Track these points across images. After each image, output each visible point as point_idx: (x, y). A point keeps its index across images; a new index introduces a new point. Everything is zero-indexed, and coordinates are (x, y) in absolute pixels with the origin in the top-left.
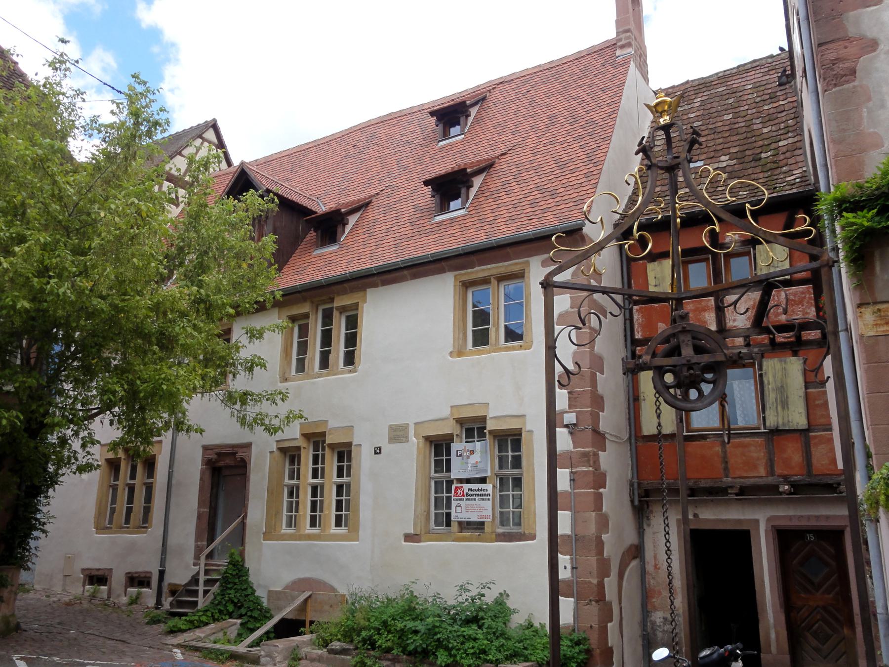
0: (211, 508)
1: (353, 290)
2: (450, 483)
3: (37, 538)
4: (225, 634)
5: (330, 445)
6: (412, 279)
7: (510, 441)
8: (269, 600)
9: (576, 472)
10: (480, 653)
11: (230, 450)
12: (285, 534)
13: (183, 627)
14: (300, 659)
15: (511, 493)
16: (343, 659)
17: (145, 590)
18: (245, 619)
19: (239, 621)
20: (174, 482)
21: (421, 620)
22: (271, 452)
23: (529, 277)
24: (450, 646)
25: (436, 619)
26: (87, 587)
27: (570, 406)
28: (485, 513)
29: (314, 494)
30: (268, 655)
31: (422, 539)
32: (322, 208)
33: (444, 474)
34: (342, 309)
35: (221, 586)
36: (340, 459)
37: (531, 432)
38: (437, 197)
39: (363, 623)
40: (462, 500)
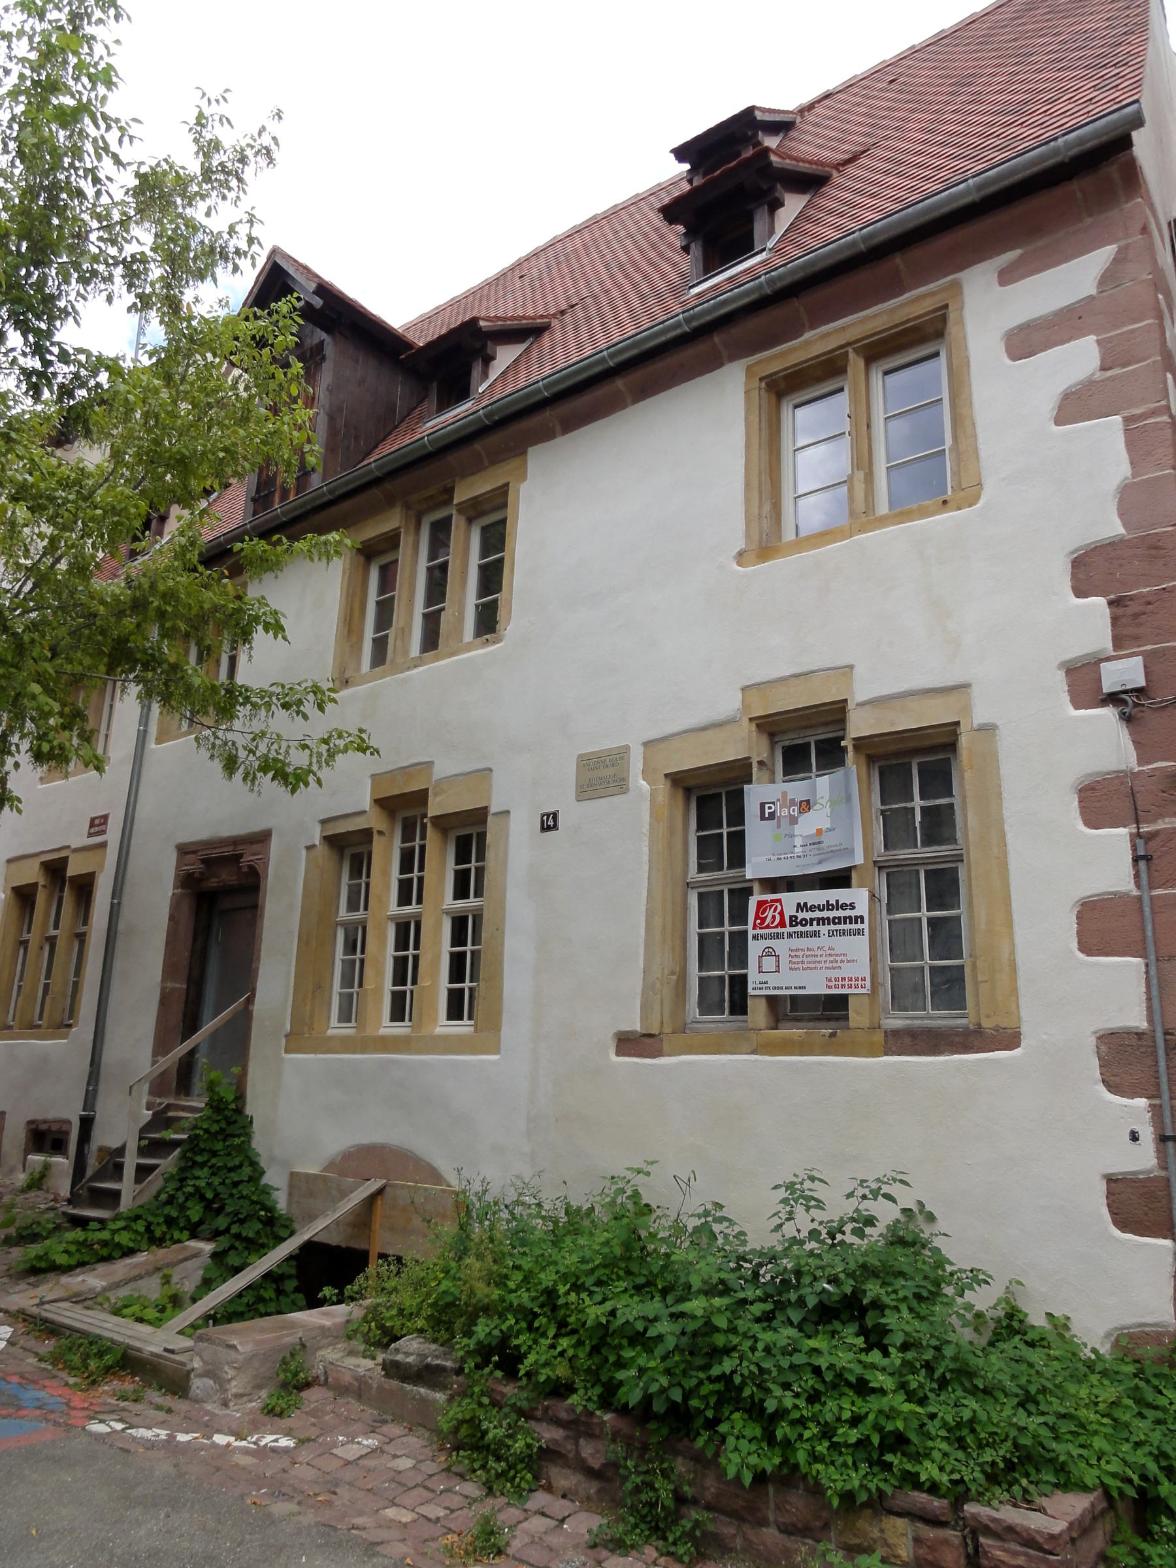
0: (189, 980)
1: (496, 458)
2: (741, 894)
4: (167, 1280)
5: (437, 820)
7: (920, 767)
8: (290, 1195)
9: (1150, 837)
10: (883, 1448)
11: (228, 851)
13: (62, 1259)
14: (307, 1385)
15: (924, 914)
16: (423, 1400)
17: (58, 1159)
18: (224, 1242)
19: (208, 1247)
20: (122, 926)
21: (664, 1292)
22: (309, 848)
24: (771, 1405)
25: (717, 1302)
27: (1119, 641)
28: (847, 971)
30: (211, 1373)
31: (666, 1047)
33: (725, 873)
34: (473, 510)
35: (183, 1156)
36: (462, 856)
37: (989, 729)
39: (486, 1293)
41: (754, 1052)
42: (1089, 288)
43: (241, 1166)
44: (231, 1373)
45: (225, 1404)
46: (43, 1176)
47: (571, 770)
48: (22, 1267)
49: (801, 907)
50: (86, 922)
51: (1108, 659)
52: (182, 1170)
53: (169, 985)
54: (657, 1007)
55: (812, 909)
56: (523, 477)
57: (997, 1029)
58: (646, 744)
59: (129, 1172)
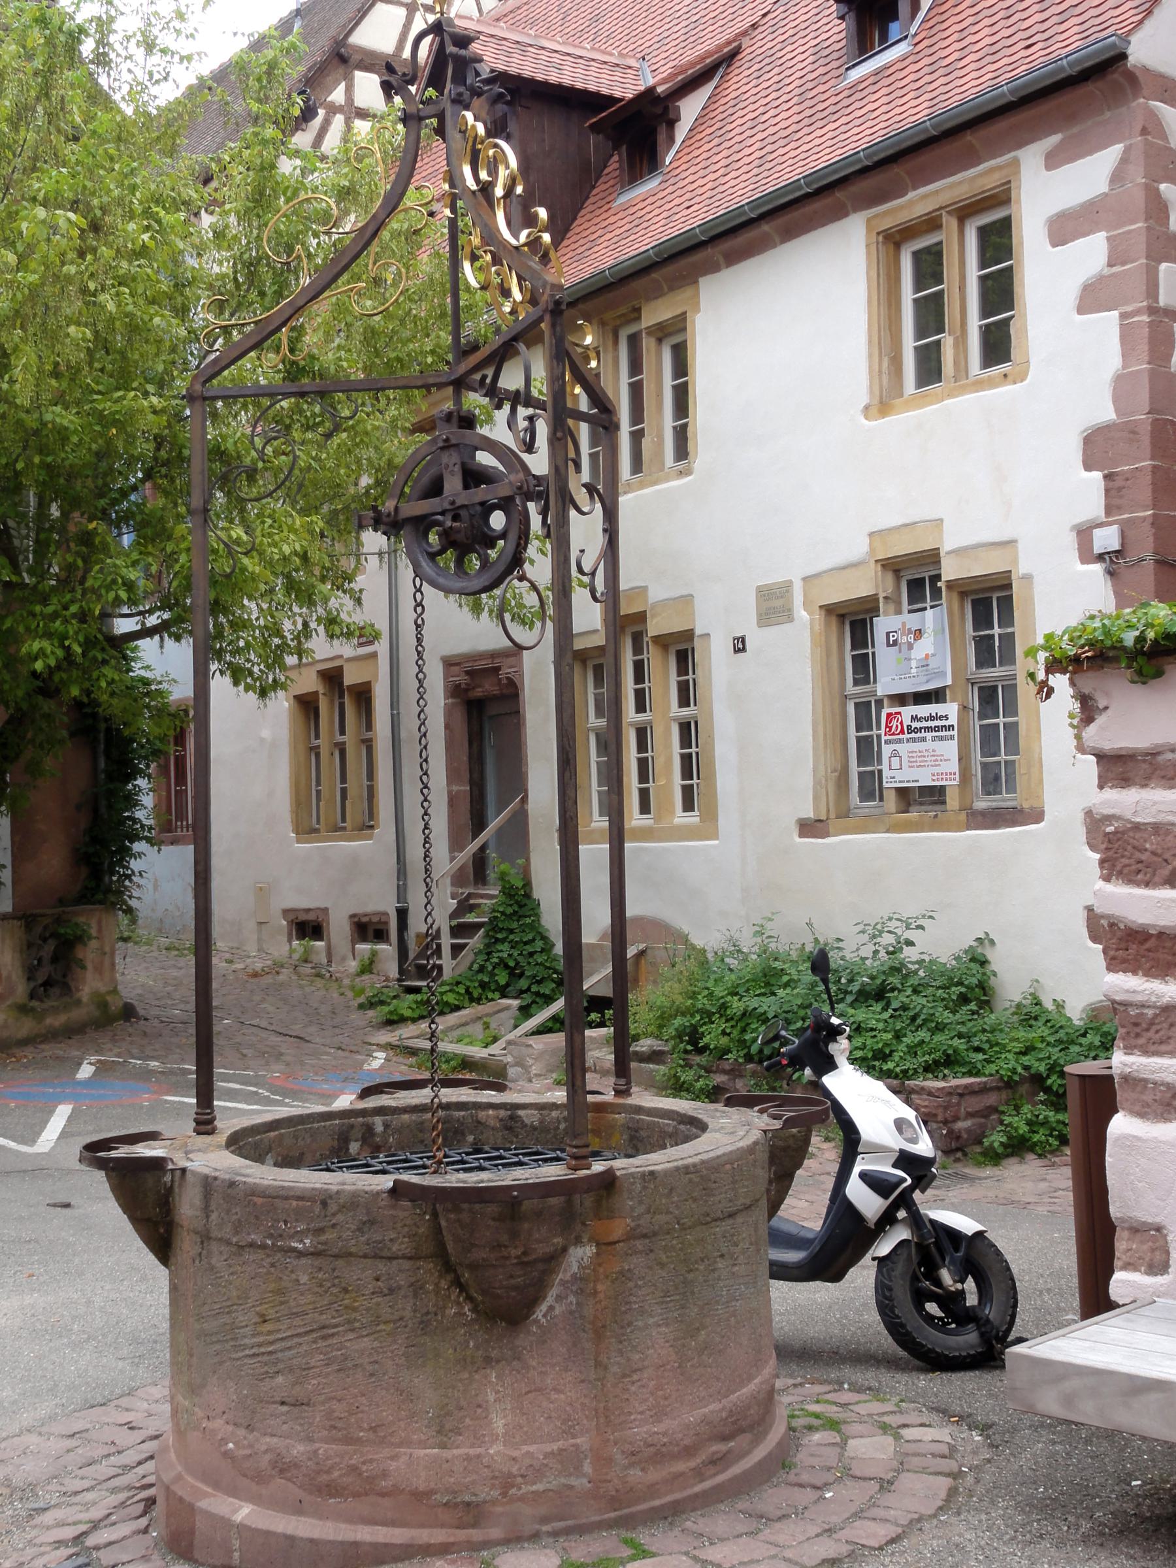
0: (472, 783)
3: (140, 855)
4: (487, 1026)
5: (657, 639)
6: (783, 241)
11: (487, 664)
12: (679, 828)
13: (407, 1013)
18: (528, 998)
19: (515, 1003)
23: (1019, 201)
26: (295, 943)
27: (1109, 510)
29: (686, 741)
31: (831, 830)
32: (625, 88)
34: (662, 332)
35: (487, 935)
36: (683, 668)
37: (1028, 578)
38: (851, 18)
40: (900, 741)
41: (887, 831)
42: (1103, 187)
43: (534, 940)
44: (531, 1062)
45: (530, 1081)
46: (372, 962)
47: (751, 601)
48: (379, 1020)
49: (914, 718)
50: (369, 727)
51: (1101, 525)
52: (487, 945)
53: (455, 788)
54: (824, 799)
55: (920, 719)
56: (697, 308)
57: (1032, 808)
58: (805, 579)
59: (446, 951)
